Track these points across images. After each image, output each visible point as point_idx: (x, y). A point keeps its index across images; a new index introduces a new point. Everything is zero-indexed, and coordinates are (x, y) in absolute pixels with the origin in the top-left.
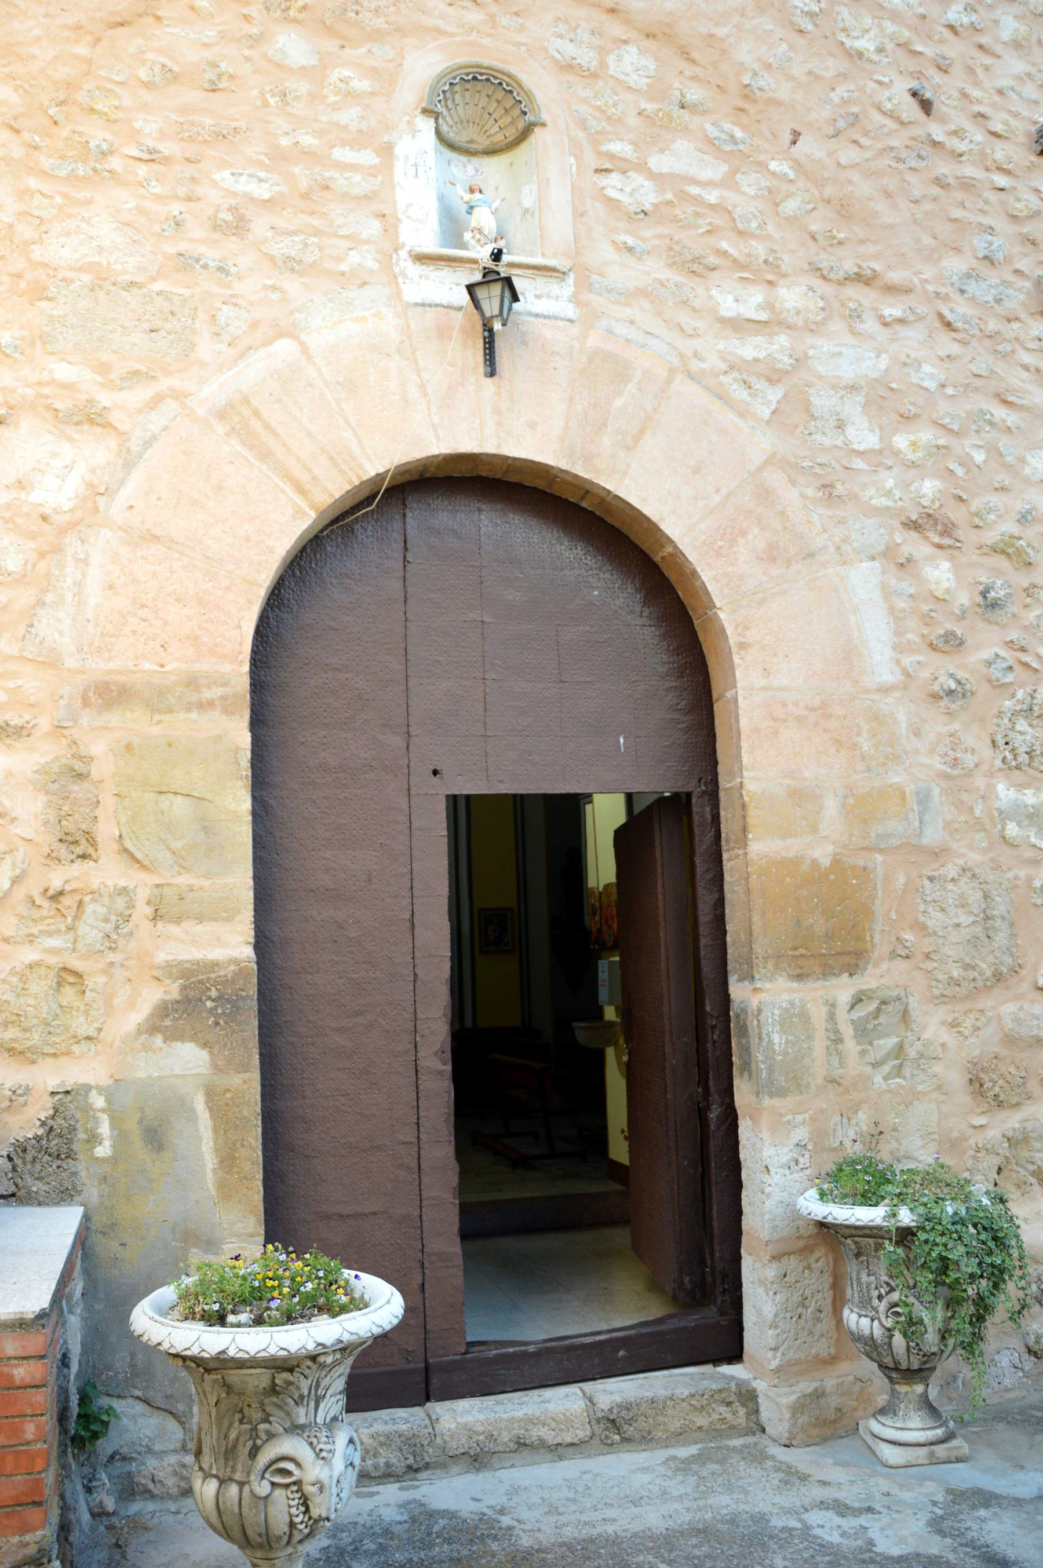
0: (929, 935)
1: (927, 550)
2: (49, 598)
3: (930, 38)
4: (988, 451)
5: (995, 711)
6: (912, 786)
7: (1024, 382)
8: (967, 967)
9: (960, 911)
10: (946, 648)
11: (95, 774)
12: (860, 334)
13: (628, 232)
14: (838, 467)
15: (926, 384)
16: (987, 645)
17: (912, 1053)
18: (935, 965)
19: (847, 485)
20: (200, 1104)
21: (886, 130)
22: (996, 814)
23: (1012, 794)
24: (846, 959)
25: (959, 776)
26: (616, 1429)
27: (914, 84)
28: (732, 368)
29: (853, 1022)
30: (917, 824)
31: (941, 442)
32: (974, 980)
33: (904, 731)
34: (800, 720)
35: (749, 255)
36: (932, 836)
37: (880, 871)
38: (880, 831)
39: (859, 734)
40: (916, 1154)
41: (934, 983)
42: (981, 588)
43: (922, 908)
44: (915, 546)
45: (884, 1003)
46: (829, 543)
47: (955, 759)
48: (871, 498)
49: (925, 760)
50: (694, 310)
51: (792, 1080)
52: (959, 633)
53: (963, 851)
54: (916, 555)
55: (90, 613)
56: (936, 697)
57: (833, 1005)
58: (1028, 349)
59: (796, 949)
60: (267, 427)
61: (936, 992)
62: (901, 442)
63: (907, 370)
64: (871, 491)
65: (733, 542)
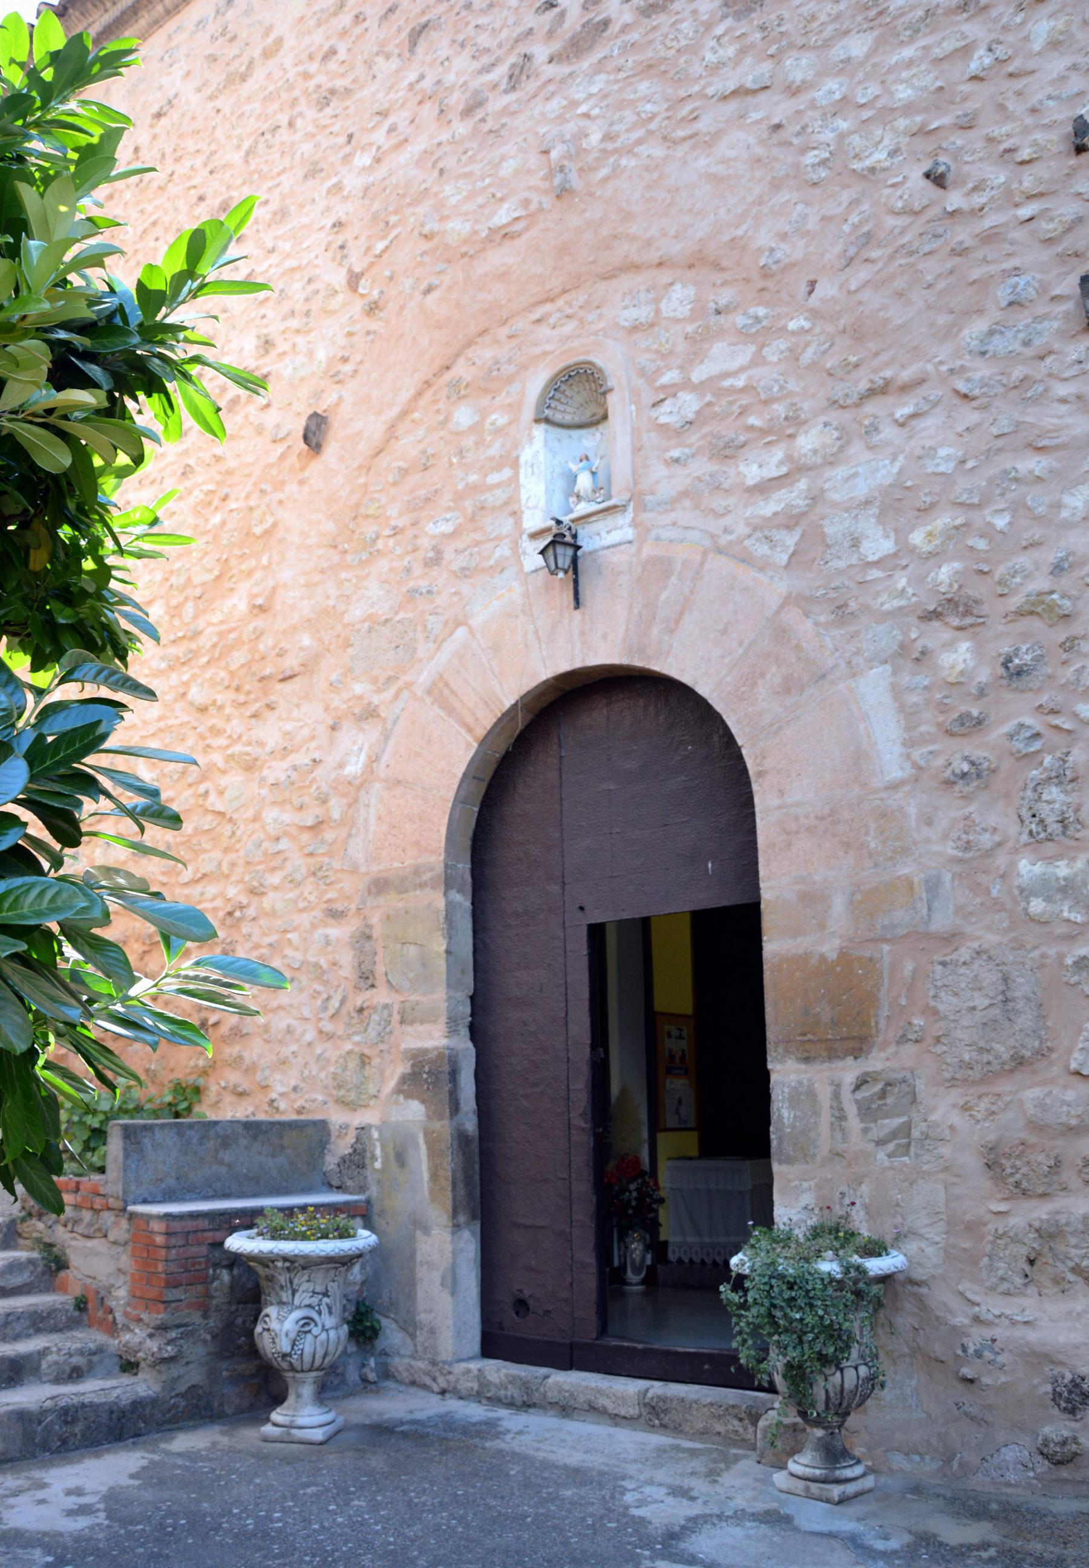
0: (942, 1019)
1: (946, 635)
2: (354, 831)
3: (953, 103)
4: (1014, 512)
5: (1020, 784)
6: (922, 875)
7: (1061, 417)
8: (981, 1050)
9: (976, 994)
10: (963, 730)
11: (375, 936)
12: (876, 446)
13: (677, 446)
14: (851, 584)
15: (942, 469)
16: (1018, 712)
17: (916, 1134)
18: (945, 1048)
19: (861, 600)
20: (421, 1140)
21: (897, 231)
22: (1016, 892)
23: (1038, 868)
24: (851, 1044)
25: (973, 859)
26: (654, 1415)
27: (926, 166)
28: (755, 529)
29: (857, 1101)
30: (925, 911)
31: (959, 521)
32: (989, 1063)
33: (913, 824)
34: (811, 830)
35: (772, 419)
36: (941, 922)
37: (886, 961)
38: (886, 922)
39: (866, 834)
40: (923, 1231)
41: (944, 1067)
42: (1002, 659)
43: (932, 993)
44: (937, 634)
45: (888, 1084)
46: (840, 661)
47: (968, 842)
48: (882, 604)
49: (935, 848)
50: (726, 491)
51: (804, 1153)
52: (975, 713)
53: (978, 933)
54: (930, 645)
55: (370, 837)
56: (949, 783)
57: (839, 1086)
58: (1066, 380)
59: (804, 1035)
60: (453, 692)
61: (947, 1075)
62: (917, 538)
63: (921, 462)
64: (884, 597)
65: (754, 684)
